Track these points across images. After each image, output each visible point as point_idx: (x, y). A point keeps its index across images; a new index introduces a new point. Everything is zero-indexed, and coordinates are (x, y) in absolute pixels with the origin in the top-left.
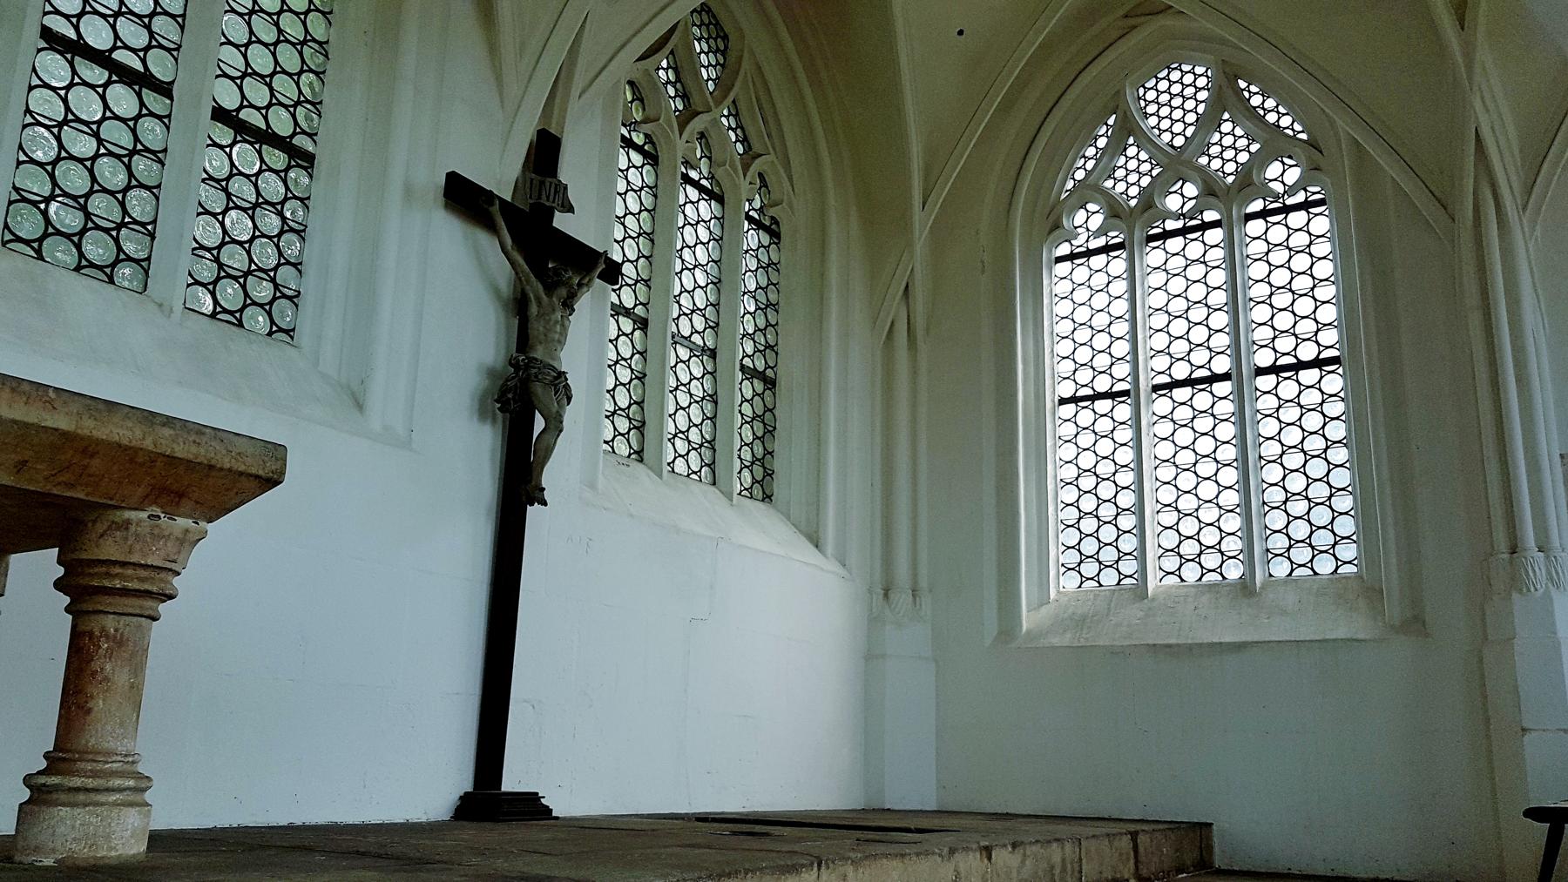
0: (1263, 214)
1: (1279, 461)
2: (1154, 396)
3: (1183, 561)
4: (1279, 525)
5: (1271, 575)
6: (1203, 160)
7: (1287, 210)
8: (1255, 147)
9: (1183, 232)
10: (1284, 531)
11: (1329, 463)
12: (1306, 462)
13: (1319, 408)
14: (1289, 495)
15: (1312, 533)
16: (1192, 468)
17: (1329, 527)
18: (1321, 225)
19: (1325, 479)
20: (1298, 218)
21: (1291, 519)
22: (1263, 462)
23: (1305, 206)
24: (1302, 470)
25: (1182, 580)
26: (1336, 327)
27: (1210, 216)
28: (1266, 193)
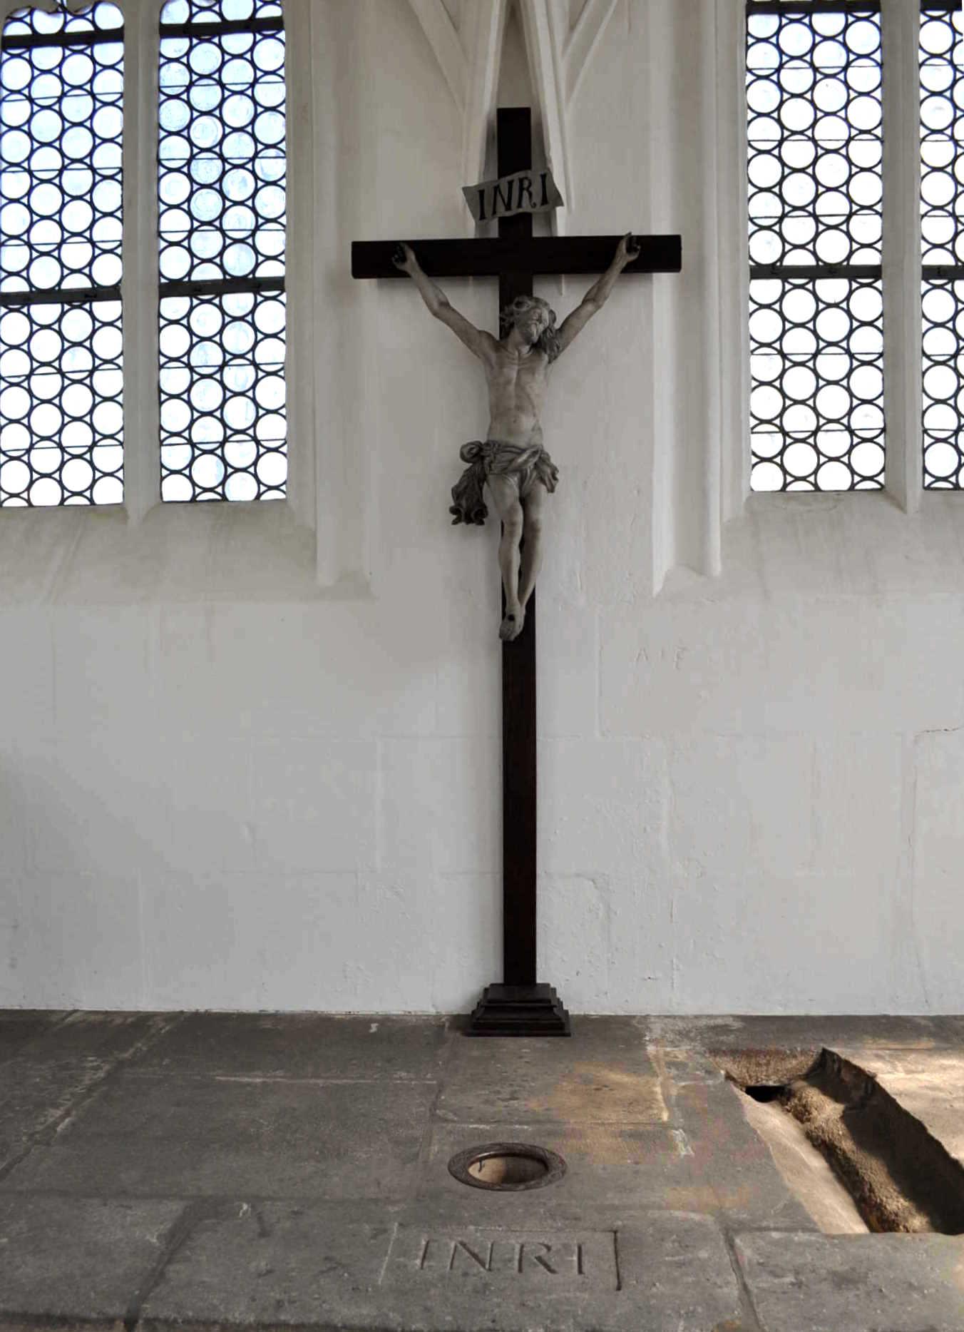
11: (818, 376)
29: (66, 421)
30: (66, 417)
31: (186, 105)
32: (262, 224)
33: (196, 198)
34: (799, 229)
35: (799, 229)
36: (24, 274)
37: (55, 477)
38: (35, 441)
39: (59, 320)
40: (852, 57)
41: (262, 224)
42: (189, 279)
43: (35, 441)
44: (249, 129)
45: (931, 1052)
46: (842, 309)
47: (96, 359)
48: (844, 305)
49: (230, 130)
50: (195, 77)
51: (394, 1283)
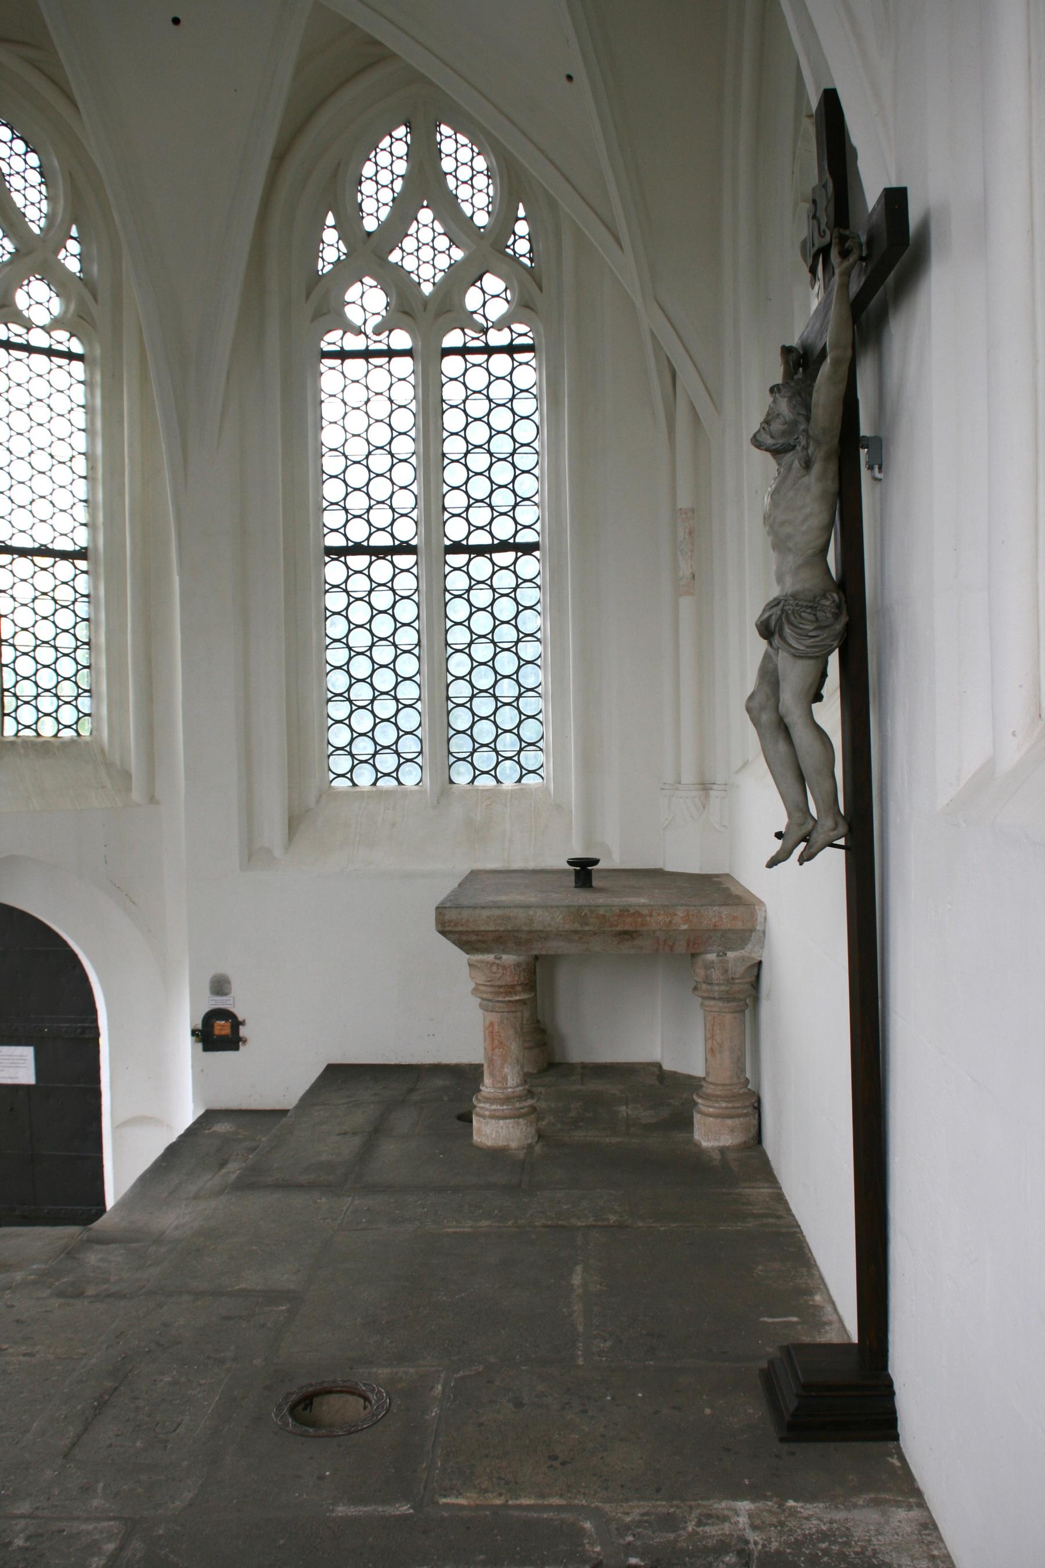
0: (463, 351)
1: (467, 651)
2: (327, 559)
3: (353, 654)
4: (462, 671)
5: (451, 782)
6: (395, 257)
7: (489, 351)
8: (458, 254)
9: (366, 354)
10: (463, 488)
11: (515, 572)
12: (493, 519)
13: (509, 404)
14: (474, 637)
15: (494, 573)
16: (369, 706)
17: (513, 622)
18: (526, 377)
19: (513, 622)
20: (500, 363)
21: (472, 528)
22: (451, 705)
23: (511, 350)
24: (490, 664)
25: (400, 783)
26: (538, 587)
27: (401, 339)
28: (465, 320)
29: (516, 419)
30: (522, 716)
31: (519, 574)
32: (521, 583)
33: (406, 739)
34: (480, 515)
35: (480, 515)
36: (512, 568)
37: (493, 378)
38: (366, 515)
39: (515, 563)
40: (521, 582)
41: (521, 583)
42: (470, 556)
43: (366, 515)
44: (355, 735)
45: (917, 1482)
46: (486, 526)
47: (403, 733)
48: (512, 568)
49: (496, 621)
50: (519, 499)
51: (858, 1535)
